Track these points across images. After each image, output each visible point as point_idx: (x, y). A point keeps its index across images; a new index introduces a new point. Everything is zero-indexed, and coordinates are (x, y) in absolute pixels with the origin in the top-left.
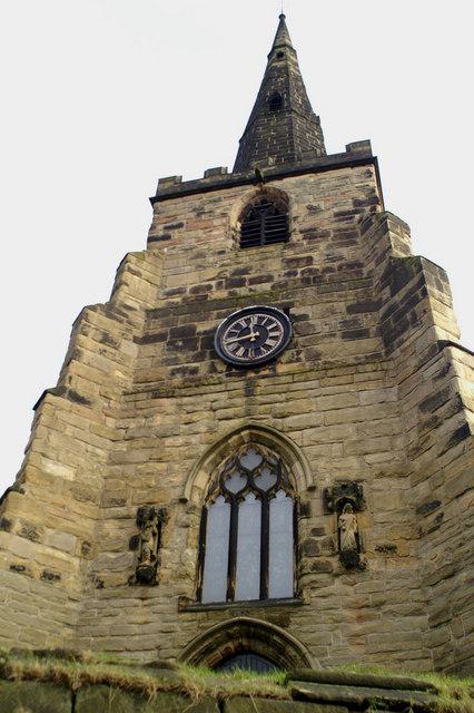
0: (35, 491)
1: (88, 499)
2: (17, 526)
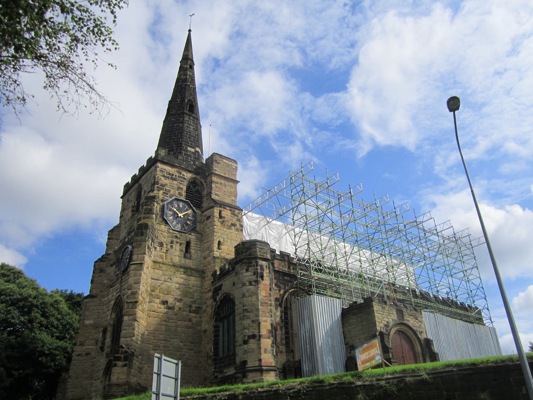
1: (97, 328)
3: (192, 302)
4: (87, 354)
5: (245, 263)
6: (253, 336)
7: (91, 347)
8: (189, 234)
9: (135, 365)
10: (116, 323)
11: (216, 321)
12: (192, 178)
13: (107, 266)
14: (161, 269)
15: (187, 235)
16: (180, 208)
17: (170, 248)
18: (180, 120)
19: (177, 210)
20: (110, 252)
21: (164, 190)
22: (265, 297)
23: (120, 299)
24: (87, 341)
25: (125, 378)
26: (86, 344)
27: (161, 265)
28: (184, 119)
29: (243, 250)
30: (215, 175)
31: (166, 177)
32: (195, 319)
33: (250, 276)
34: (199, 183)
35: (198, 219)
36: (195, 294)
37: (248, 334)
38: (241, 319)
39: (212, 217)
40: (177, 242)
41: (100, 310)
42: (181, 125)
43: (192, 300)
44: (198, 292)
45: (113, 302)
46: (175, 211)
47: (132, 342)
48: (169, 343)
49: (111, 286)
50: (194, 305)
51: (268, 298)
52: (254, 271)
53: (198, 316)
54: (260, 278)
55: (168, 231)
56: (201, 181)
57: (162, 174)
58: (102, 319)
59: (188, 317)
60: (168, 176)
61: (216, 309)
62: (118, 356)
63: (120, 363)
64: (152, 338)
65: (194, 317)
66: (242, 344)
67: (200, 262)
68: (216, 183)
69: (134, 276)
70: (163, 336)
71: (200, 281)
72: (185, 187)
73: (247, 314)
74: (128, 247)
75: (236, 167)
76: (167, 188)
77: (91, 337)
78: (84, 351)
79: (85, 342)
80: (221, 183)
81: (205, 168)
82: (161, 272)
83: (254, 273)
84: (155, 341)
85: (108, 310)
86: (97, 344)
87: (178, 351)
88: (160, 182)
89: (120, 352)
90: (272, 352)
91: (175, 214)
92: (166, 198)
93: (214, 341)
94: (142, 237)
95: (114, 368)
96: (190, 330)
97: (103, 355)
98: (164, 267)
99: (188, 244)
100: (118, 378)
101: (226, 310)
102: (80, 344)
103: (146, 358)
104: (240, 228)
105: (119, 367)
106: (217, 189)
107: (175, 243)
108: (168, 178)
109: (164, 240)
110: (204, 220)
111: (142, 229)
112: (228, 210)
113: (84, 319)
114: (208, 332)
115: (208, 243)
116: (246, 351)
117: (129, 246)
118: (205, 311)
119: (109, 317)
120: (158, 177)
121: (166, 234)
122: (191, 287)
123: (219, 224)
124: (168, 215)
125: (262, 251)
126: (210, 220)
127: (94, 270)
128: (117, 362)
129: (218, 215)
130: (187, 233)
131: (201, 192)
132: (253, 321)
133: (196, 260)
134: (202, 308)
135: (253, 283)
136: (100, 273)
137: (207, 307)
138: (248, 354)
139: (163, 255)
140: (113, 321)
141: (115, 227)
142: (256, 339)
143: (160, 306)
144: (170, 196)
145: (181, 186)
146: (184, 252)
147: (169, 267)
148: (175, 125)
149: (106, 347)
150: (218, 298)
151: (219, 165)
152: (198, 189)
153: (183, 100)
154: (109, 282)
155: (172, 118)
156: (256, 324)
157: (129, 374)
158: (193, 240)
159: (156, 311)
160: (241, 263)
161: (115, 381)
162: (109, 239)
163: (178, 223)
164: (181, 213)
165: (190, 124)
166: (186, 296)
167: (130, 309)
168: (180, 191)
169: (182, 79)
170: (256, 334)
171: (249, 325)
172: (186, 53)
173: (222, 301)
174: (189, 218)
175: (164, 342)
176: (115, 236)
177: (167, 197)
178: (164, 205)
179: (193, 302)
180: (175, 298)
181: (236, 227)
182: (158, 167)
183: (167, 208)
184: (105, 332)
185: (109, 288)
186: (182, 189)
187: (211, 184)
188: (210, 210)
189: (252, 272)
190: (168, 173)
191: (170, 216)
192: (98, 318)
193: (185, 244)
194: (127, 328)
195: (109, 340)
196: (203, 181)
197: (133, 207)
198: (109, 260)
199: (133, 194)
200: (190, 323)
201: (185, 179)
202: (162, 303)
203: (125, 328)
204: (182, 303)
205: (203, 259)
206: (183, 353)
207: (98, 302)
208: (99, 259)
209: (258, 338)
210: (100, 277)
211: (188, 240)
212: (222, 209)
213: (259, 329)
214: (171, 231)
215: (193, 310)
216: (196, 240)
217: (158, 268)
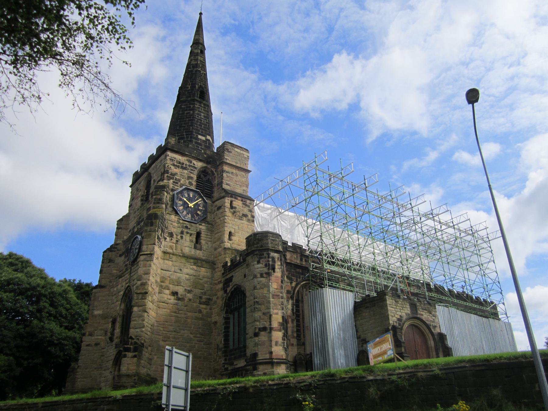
1: (106, 318)
2: (87, 333)
3: (202, 293)
4: (97, 344)
5: (257, 254)
6: (264, 329)
7: (100, 337)
8: (200, 225)
9: (144, 356)
10: (125, 313)
11: (226, 313)
14: (171, 260)
15: (198, 225)
16: (190, 197)
17: (180, 239)
18: (191, 107)
19: (187, 200)
20: (118, 242)
21: (175, 179)
23: (129, 289)
24: (96, 331)
25: (134, 369)
26: (95, 335)
27: (171, 255)
28: (194, 107)
29: (255, 242)
30: (226, 164)
31: (177, 166)
32: (205, 311)
33: (261, 268)
34: (210, 172)
35: (209, 210)
36: (206, 285)
37: (259, 327)
38: (252, 312)
39: (223, 207)
40: (187, 233)
41: (109, 300)
42: (191, 112)
43: (202, 291)
45: (122, 293)
46: (185, 201)
47: (141, 333)
48: (179, 334)
49: (120, 277)
50: (204, 297)
51: (280, 290)
52: (266, 263)
53: (209, 307)
54: (271, 270)
55: (178, 221)
56: (212, 170)
59: (198, 309)
60: (178, 164)
61: (227, 301)
62: (128, 347)
63: (130, 354)
64: (162, 329)
65: (204, 309)
66: (253, 336)
67: (210, 253)
68: (227, 172)
69: (143, 267)
71: (211, 272)
72: (196, 176)
73: (257, 306)
77: (100, 328)
78: (93, 342)
80: (232, 173)
81: (215, 157)
82: (171, 262)
83: (266, 265)
84: (164, 332)
85: (118, 301)
86: (106, 334)
87: (188, 343)
88: (170, 171)
89: (130, 343)
90: (283, 344)
91: (185, 204)
92: (176, 187)
93: (224, 332)
94: (152, 227)
95: (124, 359)
96: (200, 321)
97: (112, 345)
98: (174, 258)
99: (198, 235)
100: (128, 369)
103: (155, 349)
104: (252, 219)
105: (128, 358)
106: (228, 179)
107: (185, 234)
108: (178, 167)
109: (174, 230)
110: (215, 210)
111: (152, 219)
112: (239, 200)
113: (93, 310)
114: (218, 324)
115: (219, 234)
116: (257, 344)
118: (215, 303)
119: (118, 308)
120: (168, 166)
121: (176, 225)
122: (202, 278)
123: (230, 214)
124: (179, 205)
125: (274, 243)
126: (221, 211)
128: (127, 353)
129: (229, 205)
130: (198, 223)
131: (212, 182)
132: (264, 314)
133: (207, 250)
134: (212, 299)
135: (264, 275)
136: (109, 263)
137: (217, 298)
138: (259, 347)
140: (123, 312)
142: (267, 331)
143: (169, 297)
144: (180, 185)
145: (192, 175)
146: (195, 242)
147: (179, 257)
148: (186, 112)
149: (115, 337)
150: (229, 289)
151: (231, 154)
152: (209, 179)
153: (193, 86)
154: (117, 272)
155: (182, 105)
156: (267, 316)
157: (138, 365)
158: (203, 230)
159: (166, 302)
160: (252, 255)
161: (125, 372)
162: (117, 228)
163: (188, 214)
164: (191, 202)
165: (201, 112)
166: (196, 287)
167: (140, 300)
168: (190, 180)
169: (193, 64)
170: (267, 326)
171: (260, 317)
172: (197, 38)
173: (232, 293)
174: (200, 208)
175: (174, 333)
176: (124, 226)
177: (178, 186)
178: (174, 195)
179: (204, 294)
180: (185, 289)
181: (248, 218)
182: (168, 155)
183: (177, 198)
184: (114, 322)
185: (118, 278)
186: (192, 178)
187: (222, 174)
189: (264, 264)
190: (178, 162)
191: (180, 206)
192: (107, 308)
193: (196, 235)
194: (137, 319)
195: (118, 330)
196: (214, 170)
198: (118, 250)
200: (200, 315)
201: (196, 168)
202: (172, 294)
203: (135, 319)
204: (192, 295)
205: (213, 250)
206: (193, 344)
207: (107, 293)
208: (108, 249)
209: (269, 331)
210: (108, 267)
211: (198, 231)
212: (234, 199)
213: (270, 322)
214: (181, 221)
215: (203, 302)
216: (207, 231)
217: (168, 258)
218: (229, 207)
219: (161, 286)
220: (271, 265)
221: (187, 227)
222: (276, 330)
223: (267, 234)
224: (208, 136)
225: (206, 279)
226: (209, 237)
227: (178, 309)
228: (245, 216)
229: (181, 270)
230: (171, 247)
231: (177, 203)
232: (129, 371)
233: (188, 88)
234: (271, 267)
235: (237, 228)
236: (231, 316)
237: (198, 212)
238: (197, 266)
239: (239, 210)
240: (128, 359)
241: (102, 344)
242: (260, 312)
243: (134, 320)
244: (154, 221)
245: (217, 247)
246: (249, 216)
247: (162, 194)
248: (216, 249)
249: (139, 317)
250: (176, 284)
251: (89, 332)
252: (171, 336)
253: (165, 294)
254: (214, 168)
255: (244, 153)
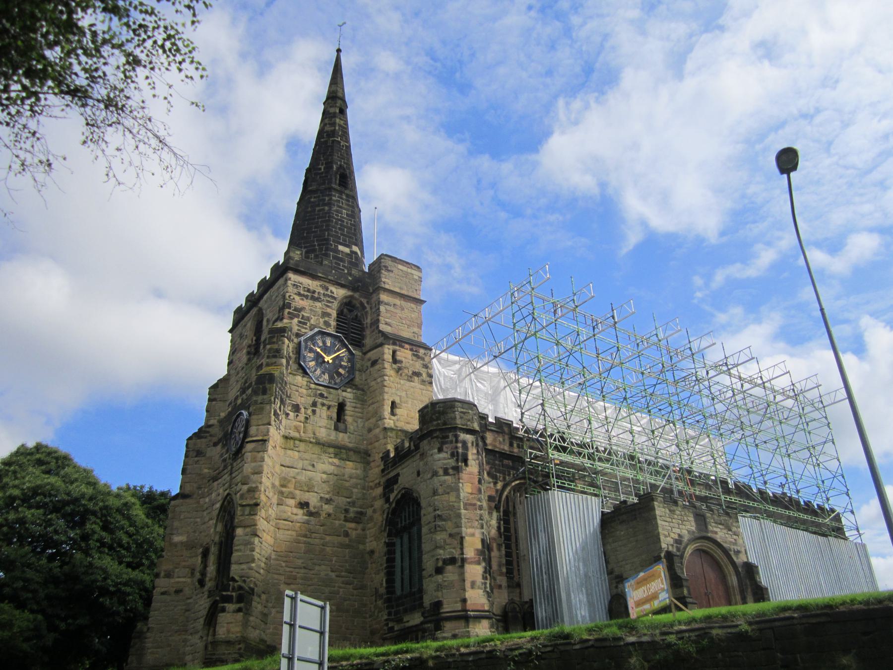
0: (169, 554)
2: (162, 574)
3: (349, 503)
4: (178, 592)
5: (437, 437)
6: (452, 561)
8: (343, 391)
10: (223, 539)
11: (389, 535)
12: (346, 297)
13: (208, 446)
14: (297, 449)
15: (340, 391)
17: (311, 414)
18: (324, 200)
19: (321, 350)
20: (212, 422)
22: (471, 494)
24: (177, 570)
26: (176, 575)
27: (297, 442)
28: (331, 199)
29: (434, 416)
31: (303, 295)
32: (354, 532)
33: (445, 459)
34: (358, 305)
36: (355, 490)
38: (431, 532)
40: (323, 405)
43: (348, 500)
44: (359, 486)
45: (218, 505)
46: (318, 353)
49: (215, 479)
50: (352, 509)
53: (360, 526)
57: (296, 291)
58: (201, 532)
60: (306, 293)
62: (227, 595)
63: (231, 607)
64: (284, 564)
66: (434, 574)
68: (386, 304)
70: (300, 561)
73: (440, 523)
74: (241, 414)
75: (419, 277)
76: (305, 314)
77: (184, 564)
79: (174, 572)
82: (296, 453)
83: (452, 455)
84: (288, 569)
85: (211, 519)
86: (193, 574)
88: (293, 304)
90: (483, 586)
91: (318, 357)
92: (303, 330)
93: (386, 568)
94: (265, 397)
96: (347, 550)
98: (302, 446)
99: (341, 407)
100: (228, 631)
101: (405, 516)
102: (165, 575)
104: (428, 379)
105: (228, 612)
107: (319, 406)
108: (307, 297)
111: (265, 383)
115: (374, 406)
117: (243, 411)
118: (371, 518)
120: (290, 296)
121: (304, 391)
122: (348, 479)
124: (308, 359)
125: (465, 417)
126: (377, 367)
127: (186, 451)
128: (226, 605)
132: (451, 535)
133: (356, 433)
135: (451, 471)
136: (196, 457)
137: (374, 511)
139: (300, 426)
141: (220, 381)
142: (457, 565)
143: (295, 510)
144: (310, 327)
145: (329, 310)
146: (335, 420)
147: (311, 445)
148: (317, 209)
149: (207, 579)
151: (391, 274)
152: (357, 316)
153: (329, 166)
155: (311, 198)
157: (245, 624)
162: (210, 400)
163: (324, 373)
164: (329, 354)
166: (338, 493)
168: (327, 319)
169: (327, 132)
170: (457, 556)
171: (445, 541)
173: (398, 502)
174: (342, 363)
175: (303, 571)
177: (306, 329)
180: (321, 498)
183: (306, 348)
184: (205, 554)
186: (329, 315)
188: (377, 350)
189: (449, 452)
192: (195, 532)
194: (242, 547)
195: (212, 568)
196: (364, 301)
197: (249, 346)
198: (211, 436)
199: (249, 325)
201: (335, 298)
206: (336, 589)
208: (195, 434)
211: (341, 400)
212: (397, 348)
213: (462, 549)
214: (313, 386)
215: (351, 518)
217: (292, 447)
218: (391, 360)
219: (282, 493)
220: (460, 454)
221: (322, 395)
222: (471, 563)
223: (453, 403)
224: (354, 247)
225: (355, 480)
226: (360, 410)
227: (310, 531)
228: (417, 374)
229: (313, 466)
230: (297, 429)
231: (305, 357)
232: (231, 635)
233: (320, 169)
234: (460, 458)
235: (403, 394)
236: (397, 541)
237: (341, 370)
238: (340, 459)
239: (408, 365)
240: (228, 615)
241: (187, 591)
242: (445, 533)
243: (237, 550)
244: (268, 386)
245: (372, 426)
246: (424, 375)
247: (280, 343)
248: (370, 430)
249: (246, 545)
250: (306, 489)
251: (165, 571)
252: (299, 575)
253: (287, 506)
254: (365, 298)
255: (413, 272)
